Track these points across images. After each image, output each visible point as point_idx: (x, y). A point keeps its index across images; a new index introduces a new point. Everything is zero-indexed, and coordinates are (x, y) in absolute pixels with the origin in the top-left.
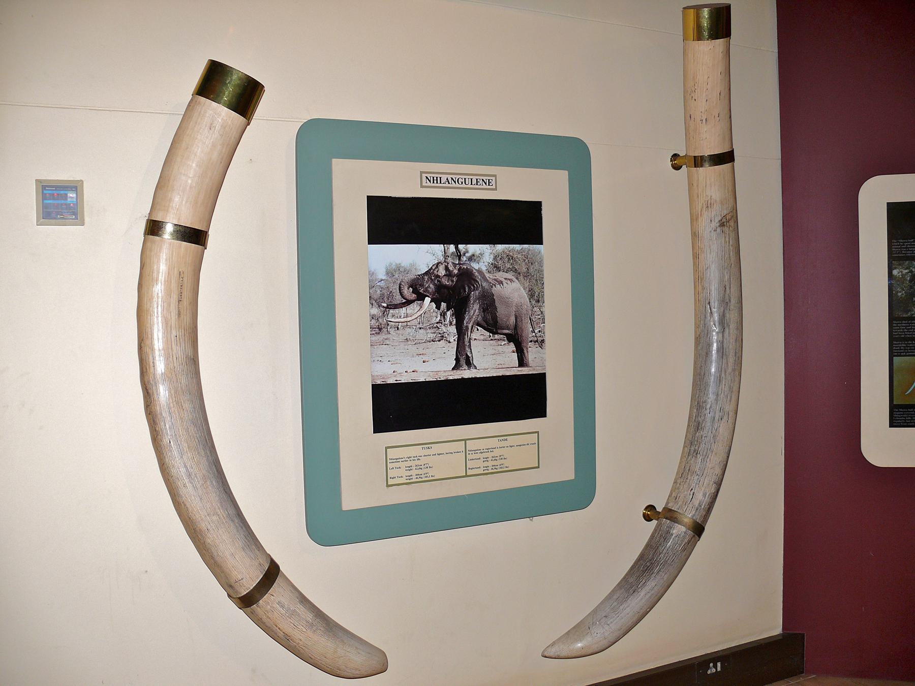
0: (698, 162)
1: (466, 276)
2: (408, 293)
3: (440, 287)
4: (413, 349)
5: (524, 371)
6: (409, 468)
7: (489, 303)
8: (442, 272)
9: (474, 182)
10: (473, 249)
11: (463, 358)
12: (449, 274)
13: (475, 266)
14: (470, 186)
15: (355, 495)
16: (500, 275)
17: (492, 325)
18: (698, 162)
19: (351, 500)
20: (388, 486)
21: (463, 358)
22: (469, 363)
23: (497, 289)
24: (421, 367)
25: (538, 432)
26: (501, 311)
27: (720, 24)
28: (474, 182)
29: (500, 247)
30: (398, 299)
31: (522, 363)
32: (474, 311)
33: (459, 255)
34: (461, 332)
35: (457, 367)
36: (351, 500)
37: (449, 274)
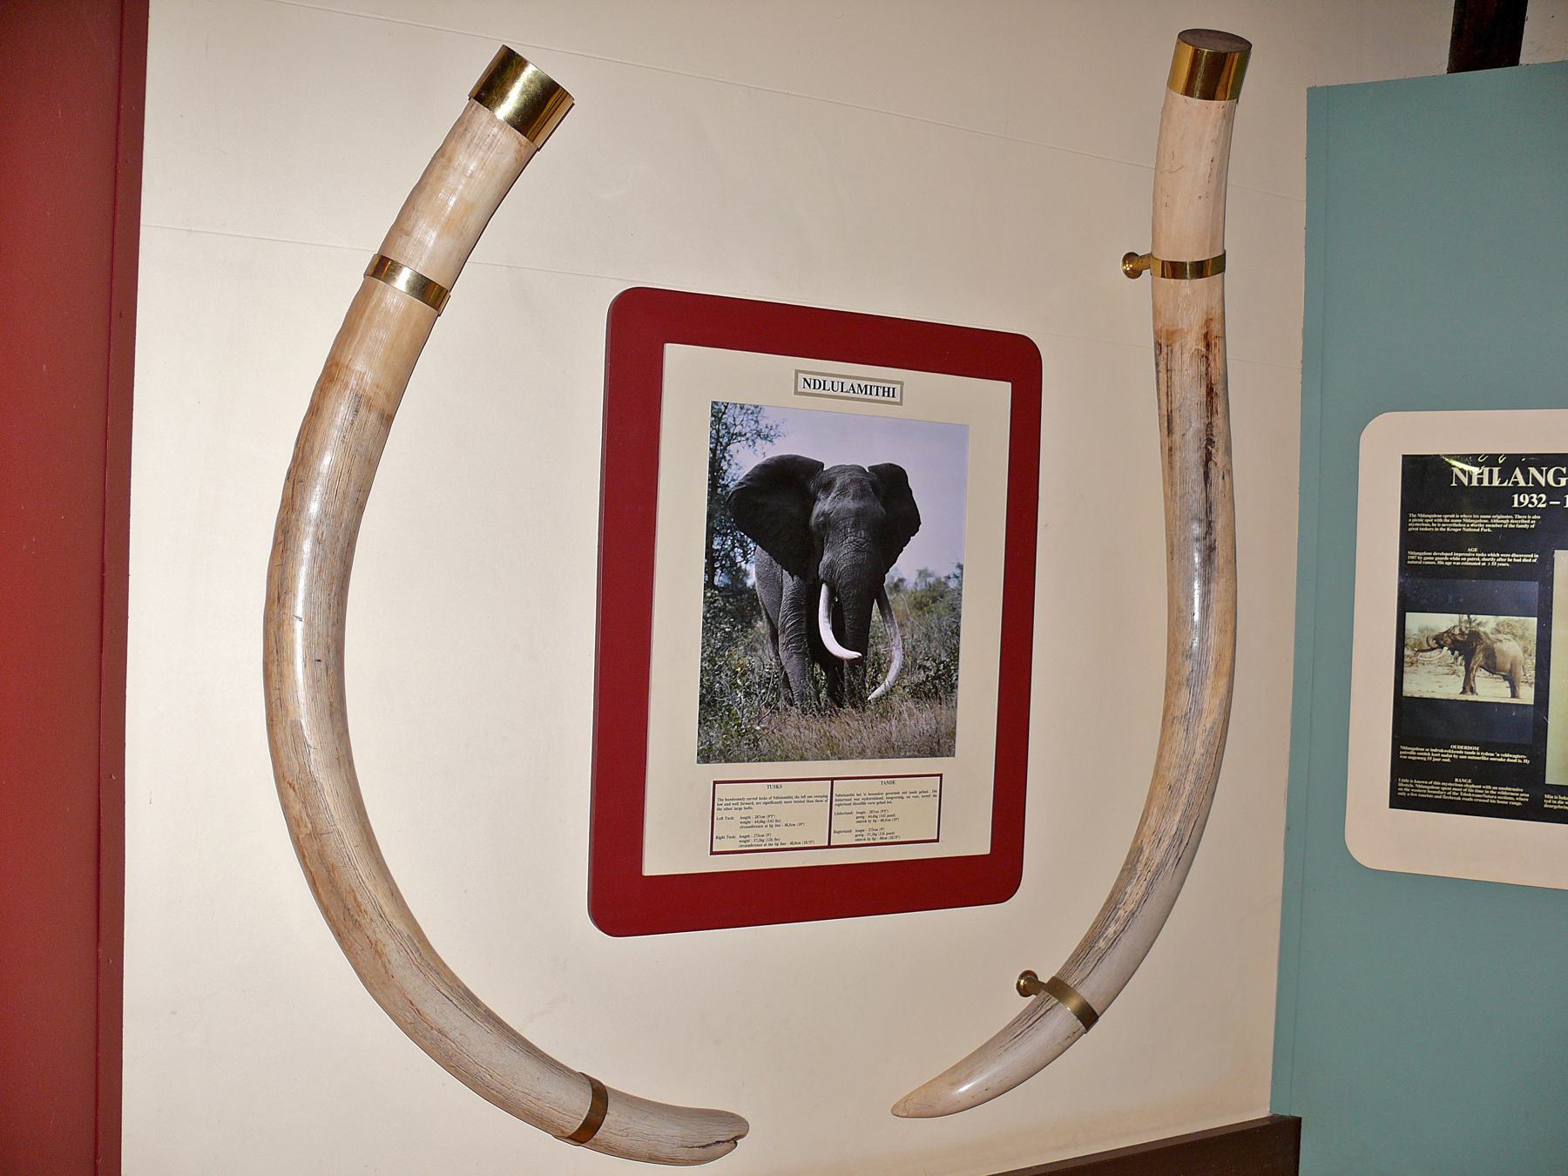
0: (1175, 270)
1: (1475, 636)
2: (1433, 643)
3: (1455, 641)
4: (1434, 679)
5: (1515, 701)
6: (861, 818)
7: (1490, 654)
8: (1457, 631)
9: (828, 385)
10: (1480, 618)
11: (1468, 686)
12: (1462, 633)
13: (1482, 629)
14: (839, 393)
15: (665, 854)
16: (1500, 636)
17: (1492, 667)
18: (1175, 270)
19: (656, 863)
20: (712, 853)
21: (1468, 686)
22: (1472, 691)
23: (1497, 646)
24: (1435, 687)
25: (712, 853)
26: (1499, 660)
27: (1215, 67)
28: (828, 385)
29: (1502, 618)
30: (1425, 647)
31: (1514, 695)
32: (1479, 658)
33: (1470, 622)
34: (1468, 671)
35: (1464, 692)
36: (656, 863)
37: (1462, 633)
